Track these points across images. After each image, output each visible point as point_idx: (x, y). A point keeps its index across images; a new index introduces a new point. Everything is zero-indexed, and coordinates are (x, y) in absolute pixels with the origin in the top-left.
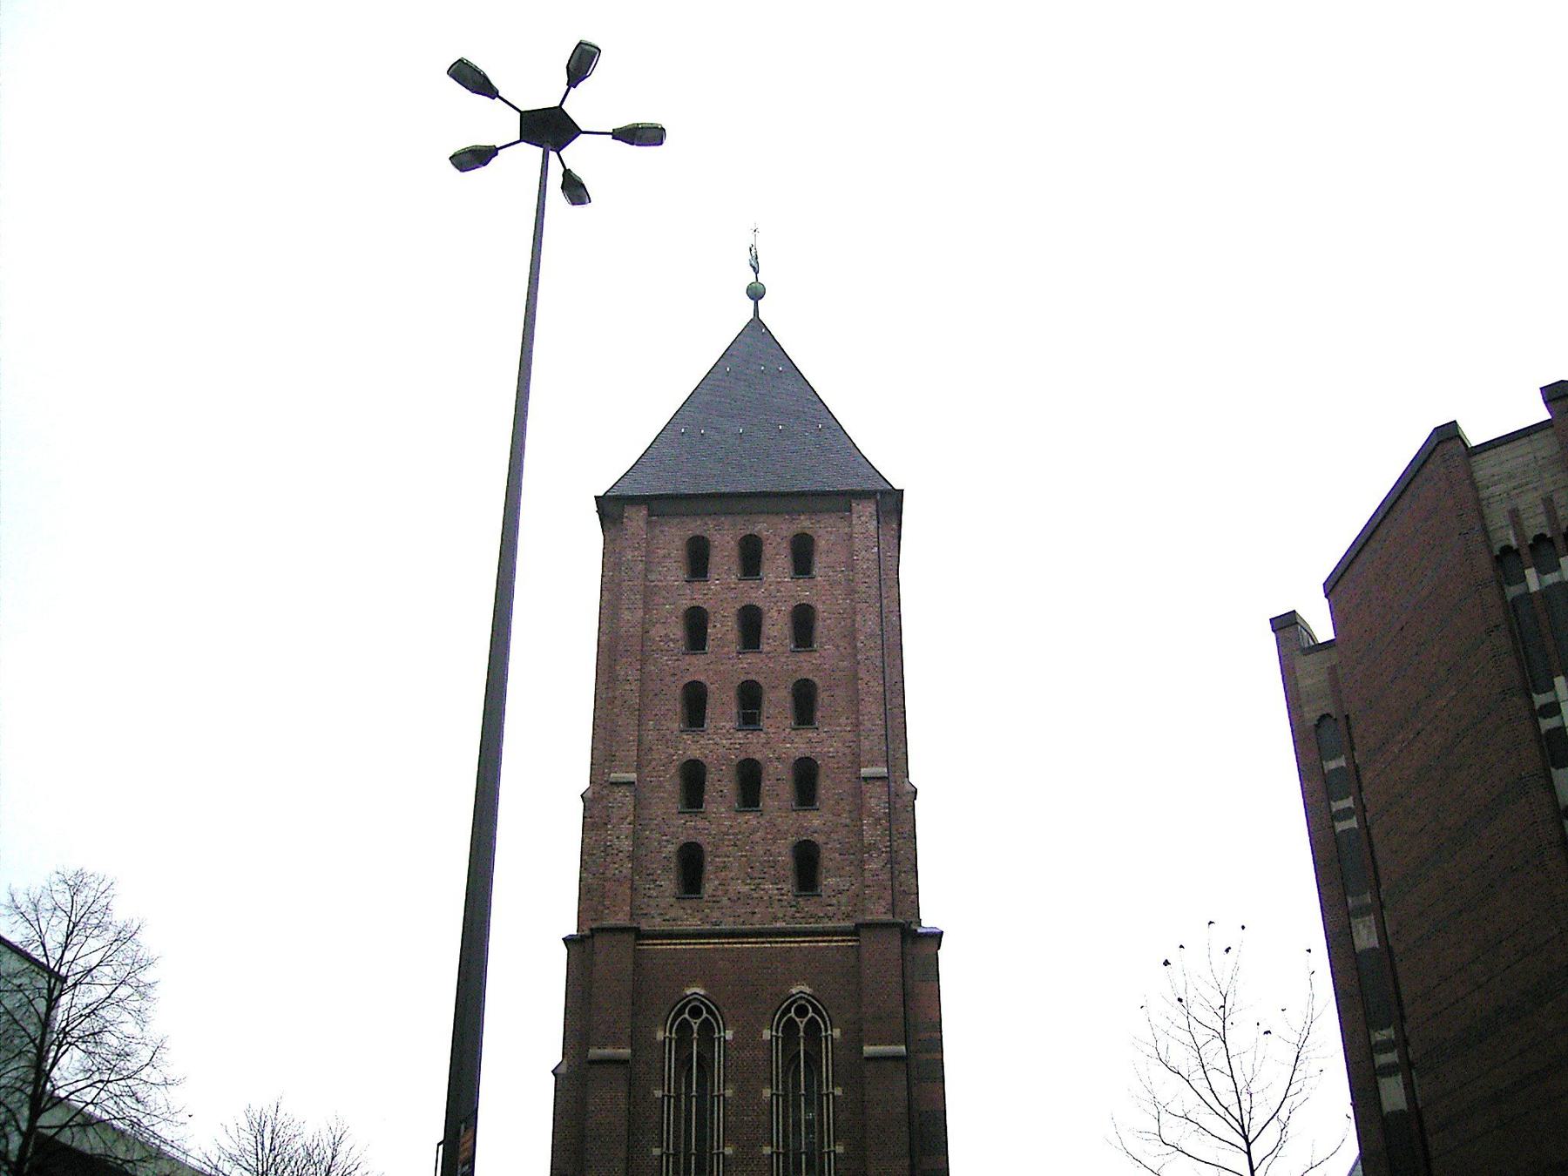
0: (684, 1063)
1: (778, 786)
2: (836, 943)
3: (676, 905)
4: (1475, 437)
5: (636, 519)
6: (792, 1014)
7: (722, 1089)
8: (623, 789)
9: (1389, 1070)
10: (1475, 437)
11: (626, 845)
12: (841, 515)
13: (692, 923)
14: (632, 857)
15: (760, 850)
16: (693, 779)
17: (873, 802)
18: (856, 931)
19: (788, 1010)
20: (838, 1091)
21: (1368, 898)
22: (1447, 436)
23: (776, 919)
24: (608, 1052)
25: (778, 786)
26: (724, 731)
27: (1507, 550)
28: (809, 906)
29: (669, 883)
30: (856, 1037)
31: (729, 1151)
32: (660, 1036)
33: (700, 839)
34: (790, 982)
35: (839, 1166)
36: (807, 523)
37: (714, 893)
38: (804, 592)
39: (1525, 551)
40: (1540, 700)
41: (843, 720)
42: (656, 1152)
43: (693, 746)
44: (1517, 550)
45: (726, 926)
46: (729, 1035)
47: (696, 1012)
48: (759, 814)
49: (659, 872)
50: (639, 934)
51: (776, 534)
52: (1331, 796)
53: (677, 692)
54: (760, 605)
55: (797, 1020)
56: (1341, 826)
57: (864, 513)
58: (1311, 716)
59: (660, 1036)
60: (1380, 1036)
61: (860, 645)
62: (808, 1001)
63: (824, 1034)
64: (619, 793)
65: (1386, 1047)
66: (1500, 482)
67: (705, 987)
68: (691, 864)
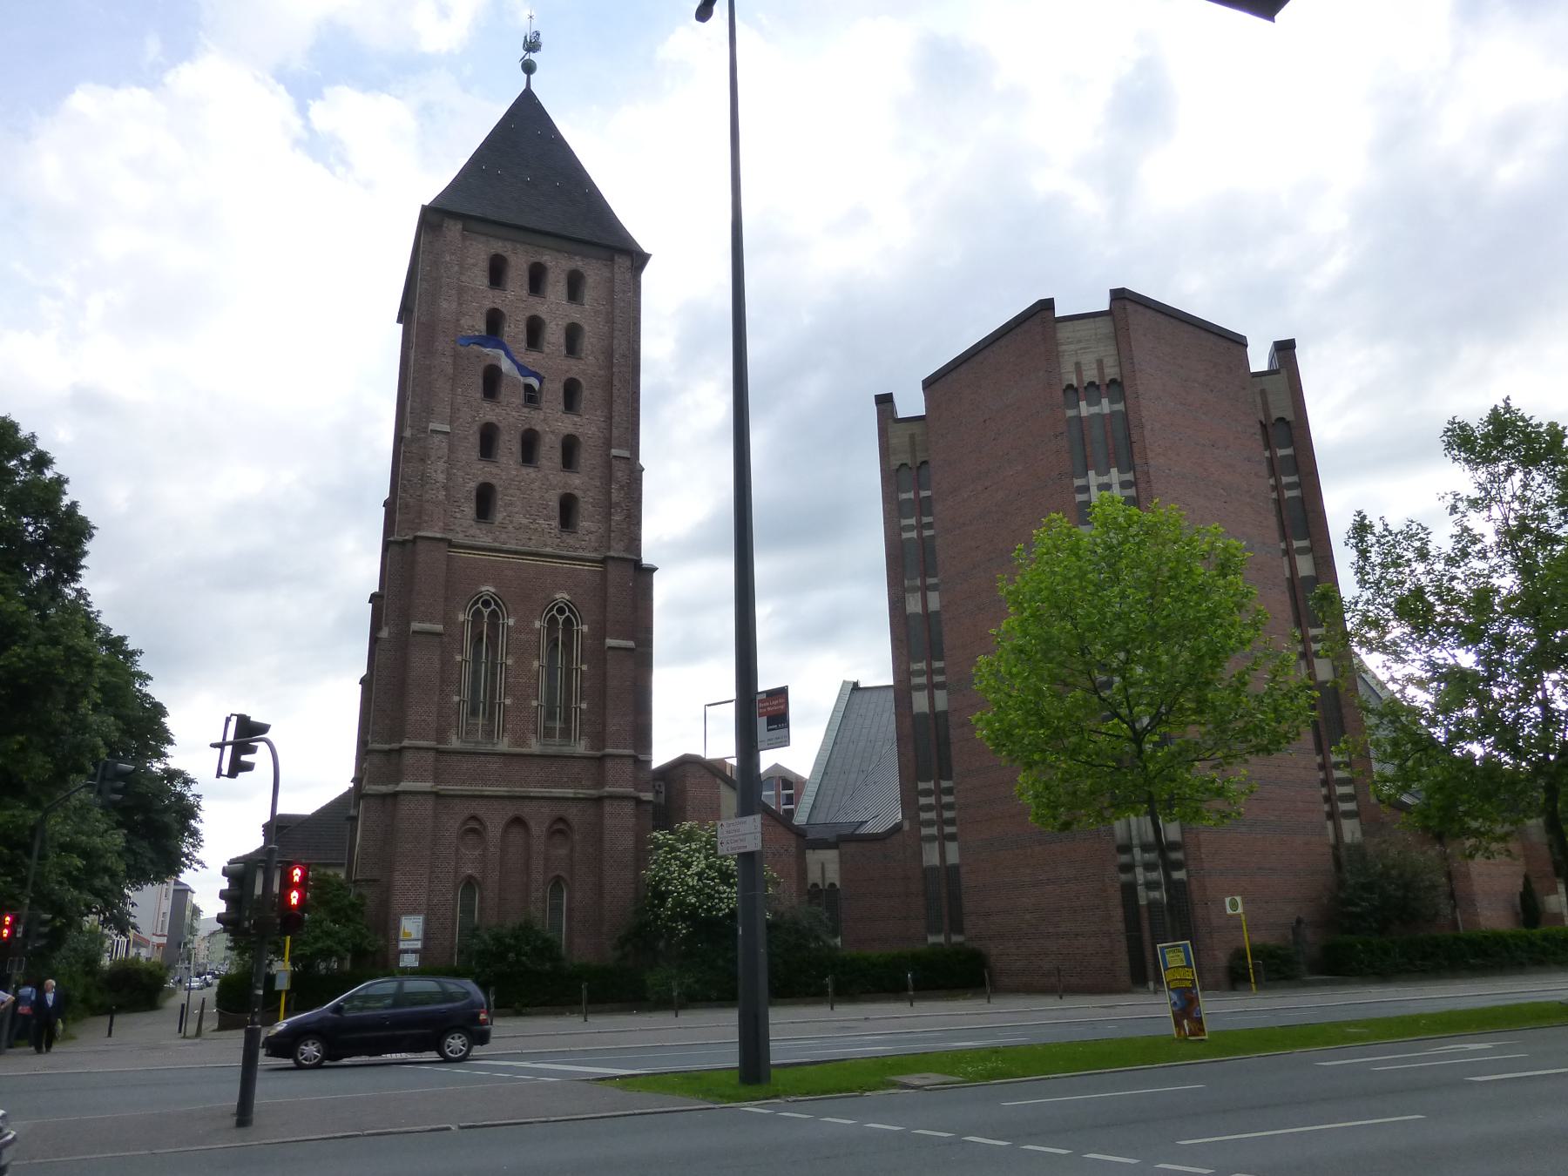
0: (477, 640)
1: (549, 451)
2: (587, 567)
3: (475, 526)
4: (1060, 312)
5: (453, 230)
6: (555, 612)
7: (504, 658)
8: (440, 437)
9: (919, 688)
10: (1060, 312)
11: (441, 477)
12: (604, 262)
13: (485, 540)
14: (446, 488)
15: (536, 495)
16: (488, 440)
17: (619, 474)
18: (604, 561)
19: (476, 602)
20: (585, 667)
21: (918, 582)
22: (1047, 305)
23: (546, 545)
24: (427, 626)
25: (549, 451)
26: (514, 406)
27: (1070, 387)
28: (570, 540)
29: (470, 509)
30: (600, 632)
31: (508, 702)
32: (461, 618)
33: (494, 481)
34: (485, 582)
35: (583, 717)
36: (545, 258)
37: (503, 521)
38: (575, 314)
39: (1081, 390)
40: (1078, 482)
41: (598, 413)
42: (456, 699)
43: (489, 413)
44: (1099, 386)
45: (512, 546)
46: (511, 622)
47: (486, 604)
48: (536, 470)
49: (463, 501)
50: (450, 544)
51: (558, 266)
52: (902, 515)
53: (480, 370)
54: (544, 317)
55: (558, 616)
56: (906, 535)
57: (622, 262)
58: (895, 463)
59: (461, 618)
60: (916, 666)
61: (615, 361)
62: (566, 604)
63: (575, 628)
64: (437, 439)
65: (920, 673)
66: (1071, 343)
67: (495, 587)
68: (485, 499)
